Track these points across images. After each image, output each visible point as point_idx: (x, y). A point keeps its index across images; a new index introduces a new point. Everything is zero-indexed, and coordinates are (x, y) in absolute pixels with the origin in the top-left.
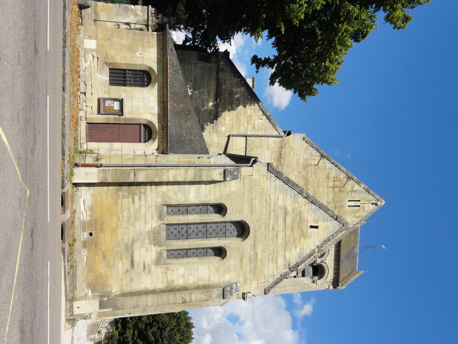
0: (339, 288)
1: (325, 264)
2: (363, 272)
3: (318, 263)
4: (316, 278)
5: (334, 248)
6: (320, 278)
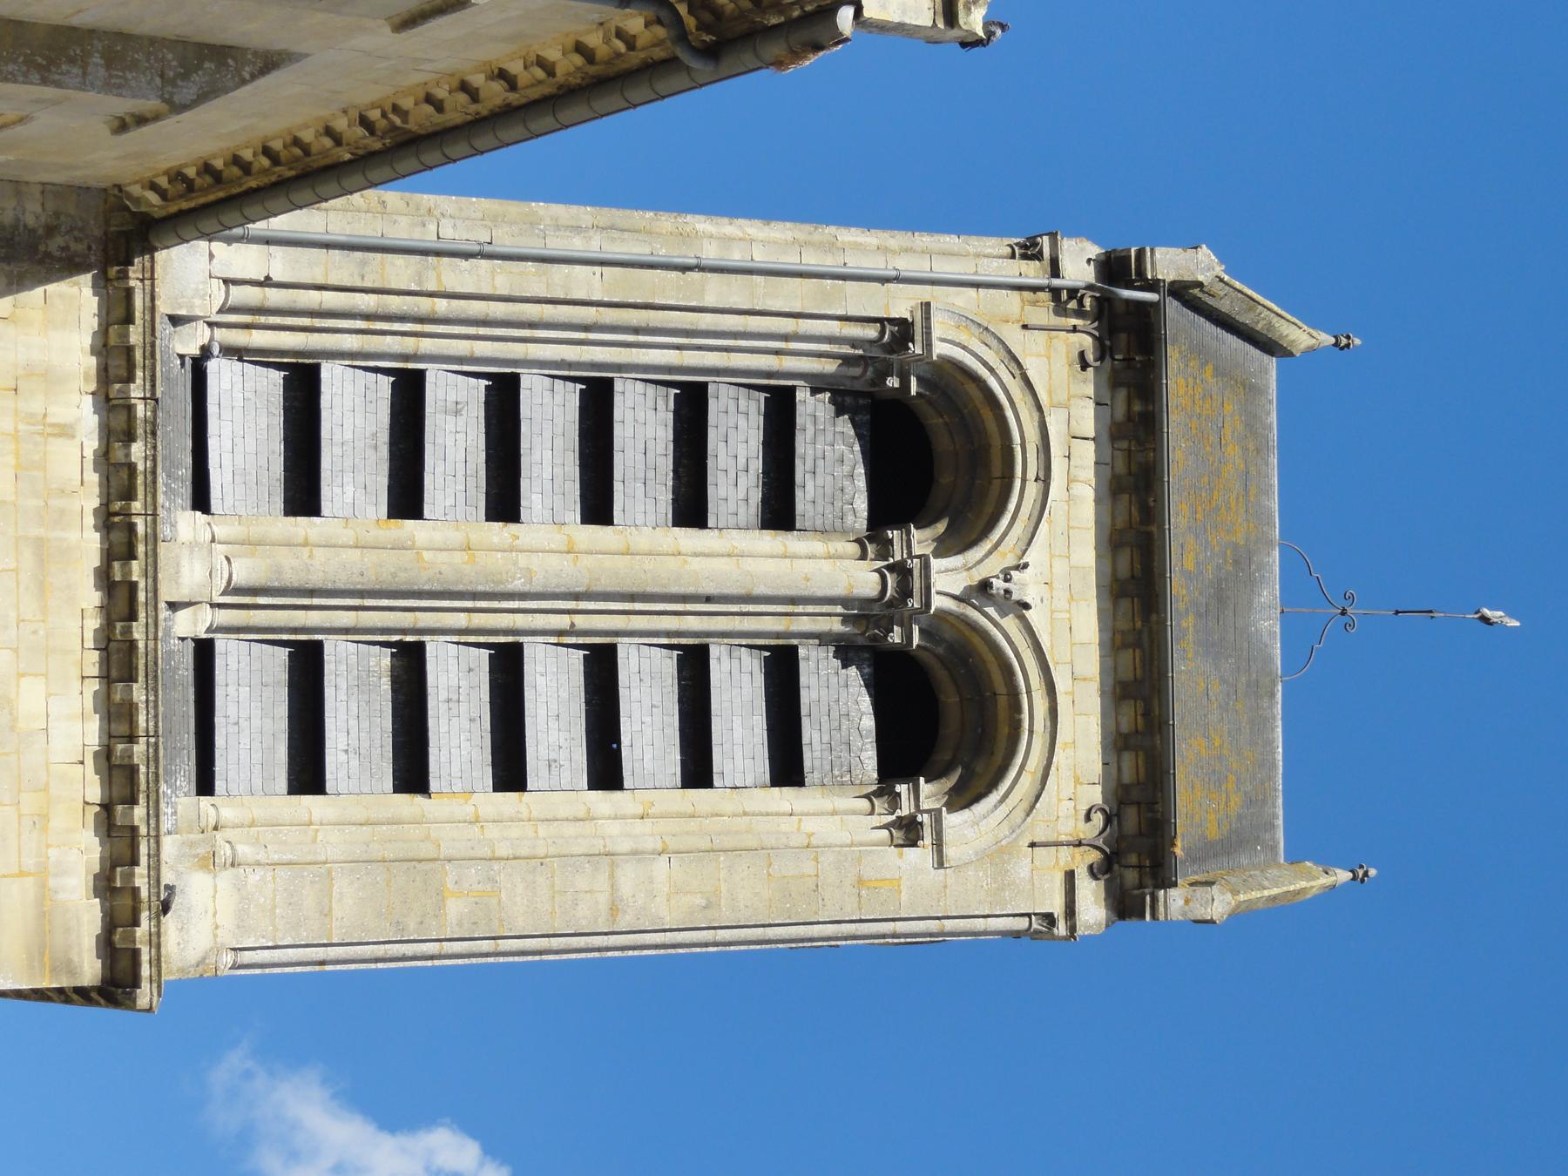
0: (1176, 902)
1: (1010, 623)
2: (1344, 876)
3: (938, 602)
4: (930, 793)
5: (1087, 454)
6: (963, 797)
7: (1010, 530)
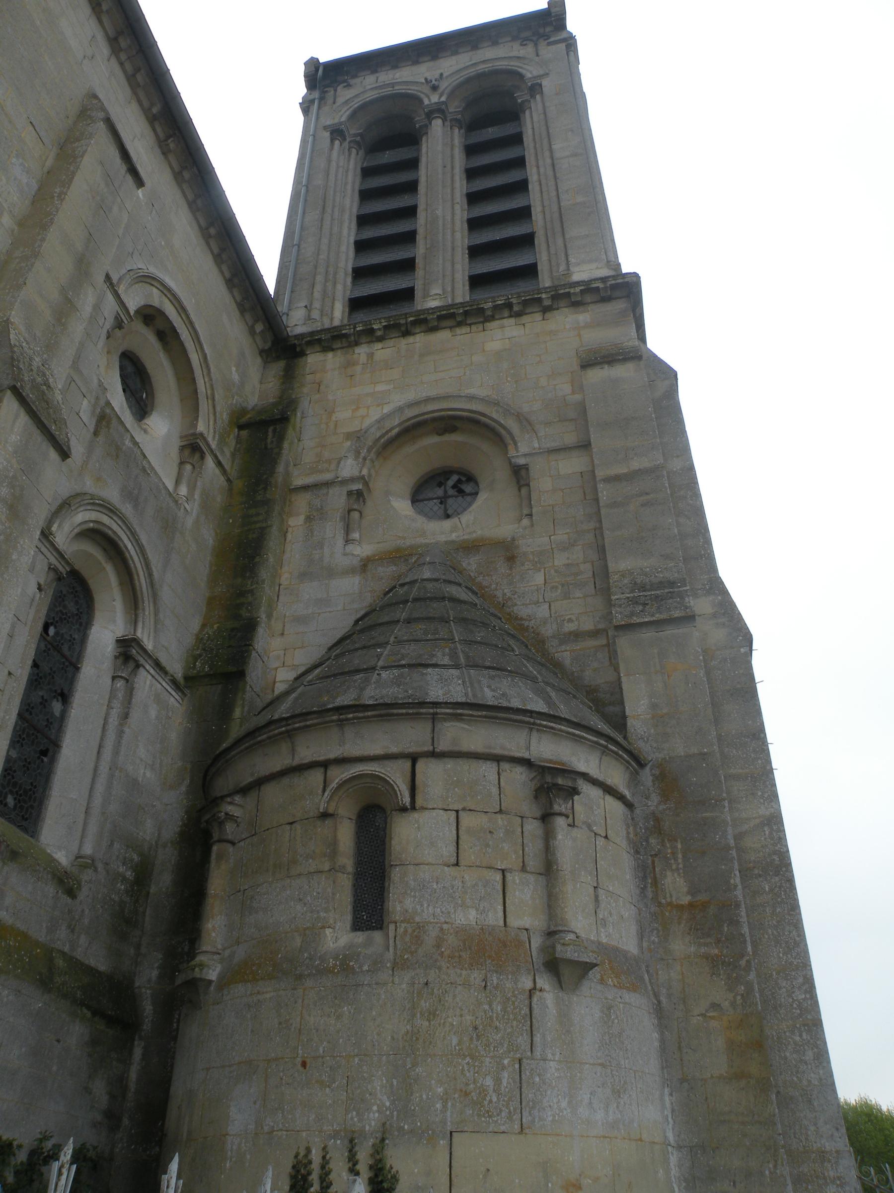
7: (412, 90)
